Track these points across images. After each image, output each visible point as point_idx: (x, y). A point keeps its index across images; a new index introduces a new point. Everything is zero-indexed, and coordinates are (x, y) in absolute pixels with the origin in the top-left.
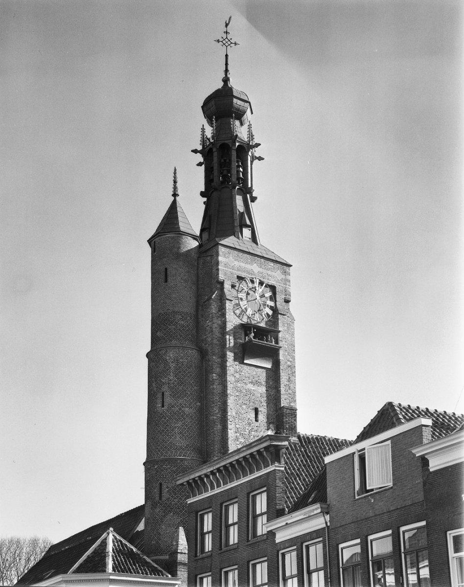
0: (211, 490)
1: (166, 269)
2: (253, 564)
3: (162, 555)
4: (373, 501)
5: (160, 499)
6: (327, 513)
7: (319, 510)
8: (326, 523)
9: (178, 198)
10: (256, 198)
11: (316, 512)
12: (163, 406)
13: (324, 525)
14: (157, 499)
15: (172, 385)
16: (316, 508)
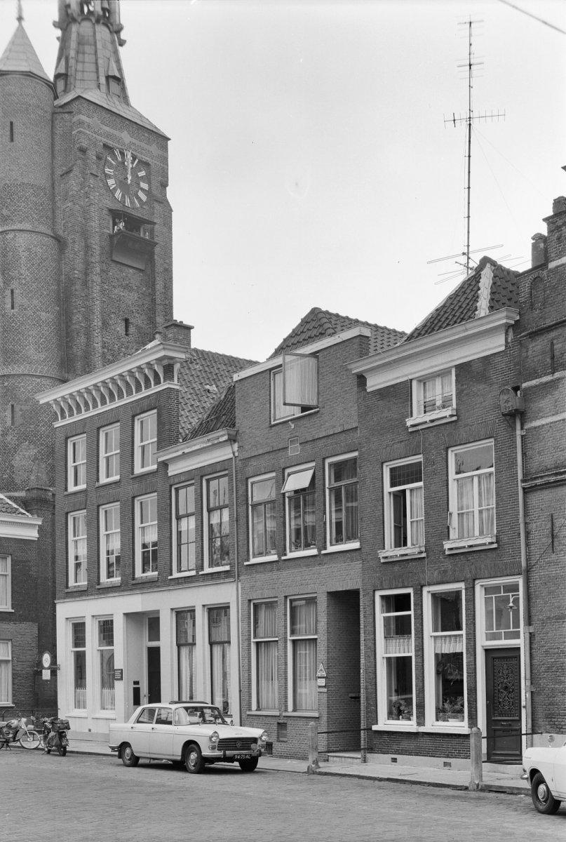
0: (93, 408)
1: (12, 123)
2: (175, 488)
3: (16, 491)
4: (293, 427)
5: (13, 423)
6: (235, 441)
7: (225, 438)
8: (234, 453)
9: (24, 23)
10: (125, 42)
11: (221, 439)
12: (13, 308)
13: (231, 456)
14: (9, 423)
15: (24, 282)
16: (222, 434)
